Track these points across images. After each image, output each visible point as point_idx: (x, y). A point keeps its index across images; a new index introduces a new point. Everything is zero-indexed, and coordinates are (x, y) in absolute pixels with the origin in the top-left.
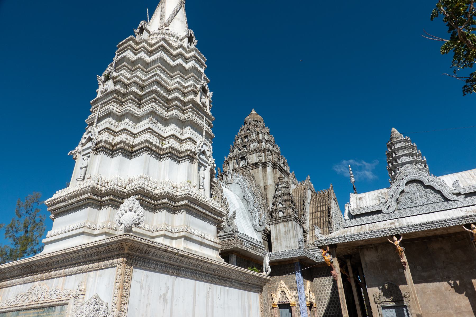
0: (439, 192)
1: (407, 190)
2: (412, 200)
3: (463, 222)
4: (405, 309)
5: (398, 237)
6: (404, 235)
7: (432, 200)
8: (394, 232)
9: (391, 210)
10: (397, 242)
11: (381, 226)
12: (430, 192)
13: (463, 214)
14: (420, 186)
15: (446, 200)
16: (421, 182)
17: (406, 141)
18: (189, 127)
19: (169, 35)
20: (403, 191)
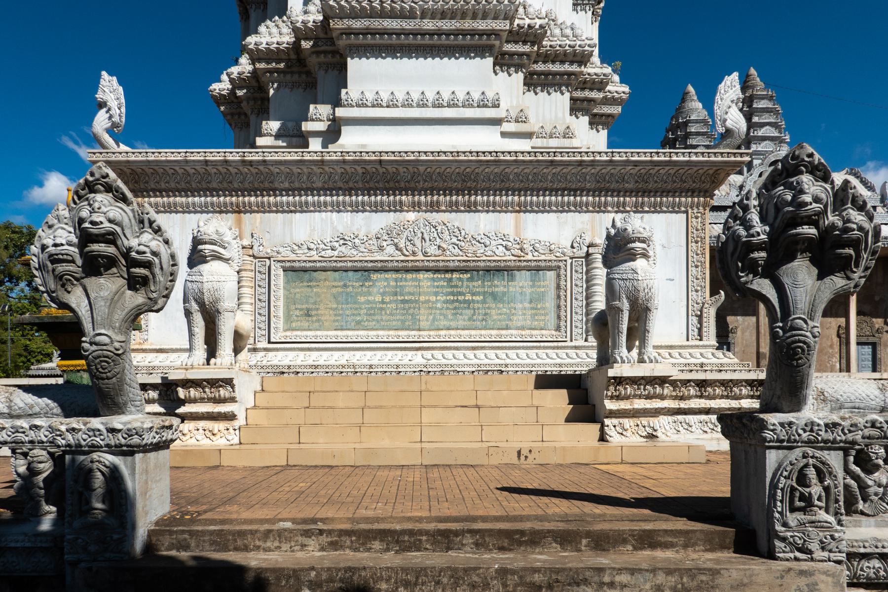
17: (770, 98)
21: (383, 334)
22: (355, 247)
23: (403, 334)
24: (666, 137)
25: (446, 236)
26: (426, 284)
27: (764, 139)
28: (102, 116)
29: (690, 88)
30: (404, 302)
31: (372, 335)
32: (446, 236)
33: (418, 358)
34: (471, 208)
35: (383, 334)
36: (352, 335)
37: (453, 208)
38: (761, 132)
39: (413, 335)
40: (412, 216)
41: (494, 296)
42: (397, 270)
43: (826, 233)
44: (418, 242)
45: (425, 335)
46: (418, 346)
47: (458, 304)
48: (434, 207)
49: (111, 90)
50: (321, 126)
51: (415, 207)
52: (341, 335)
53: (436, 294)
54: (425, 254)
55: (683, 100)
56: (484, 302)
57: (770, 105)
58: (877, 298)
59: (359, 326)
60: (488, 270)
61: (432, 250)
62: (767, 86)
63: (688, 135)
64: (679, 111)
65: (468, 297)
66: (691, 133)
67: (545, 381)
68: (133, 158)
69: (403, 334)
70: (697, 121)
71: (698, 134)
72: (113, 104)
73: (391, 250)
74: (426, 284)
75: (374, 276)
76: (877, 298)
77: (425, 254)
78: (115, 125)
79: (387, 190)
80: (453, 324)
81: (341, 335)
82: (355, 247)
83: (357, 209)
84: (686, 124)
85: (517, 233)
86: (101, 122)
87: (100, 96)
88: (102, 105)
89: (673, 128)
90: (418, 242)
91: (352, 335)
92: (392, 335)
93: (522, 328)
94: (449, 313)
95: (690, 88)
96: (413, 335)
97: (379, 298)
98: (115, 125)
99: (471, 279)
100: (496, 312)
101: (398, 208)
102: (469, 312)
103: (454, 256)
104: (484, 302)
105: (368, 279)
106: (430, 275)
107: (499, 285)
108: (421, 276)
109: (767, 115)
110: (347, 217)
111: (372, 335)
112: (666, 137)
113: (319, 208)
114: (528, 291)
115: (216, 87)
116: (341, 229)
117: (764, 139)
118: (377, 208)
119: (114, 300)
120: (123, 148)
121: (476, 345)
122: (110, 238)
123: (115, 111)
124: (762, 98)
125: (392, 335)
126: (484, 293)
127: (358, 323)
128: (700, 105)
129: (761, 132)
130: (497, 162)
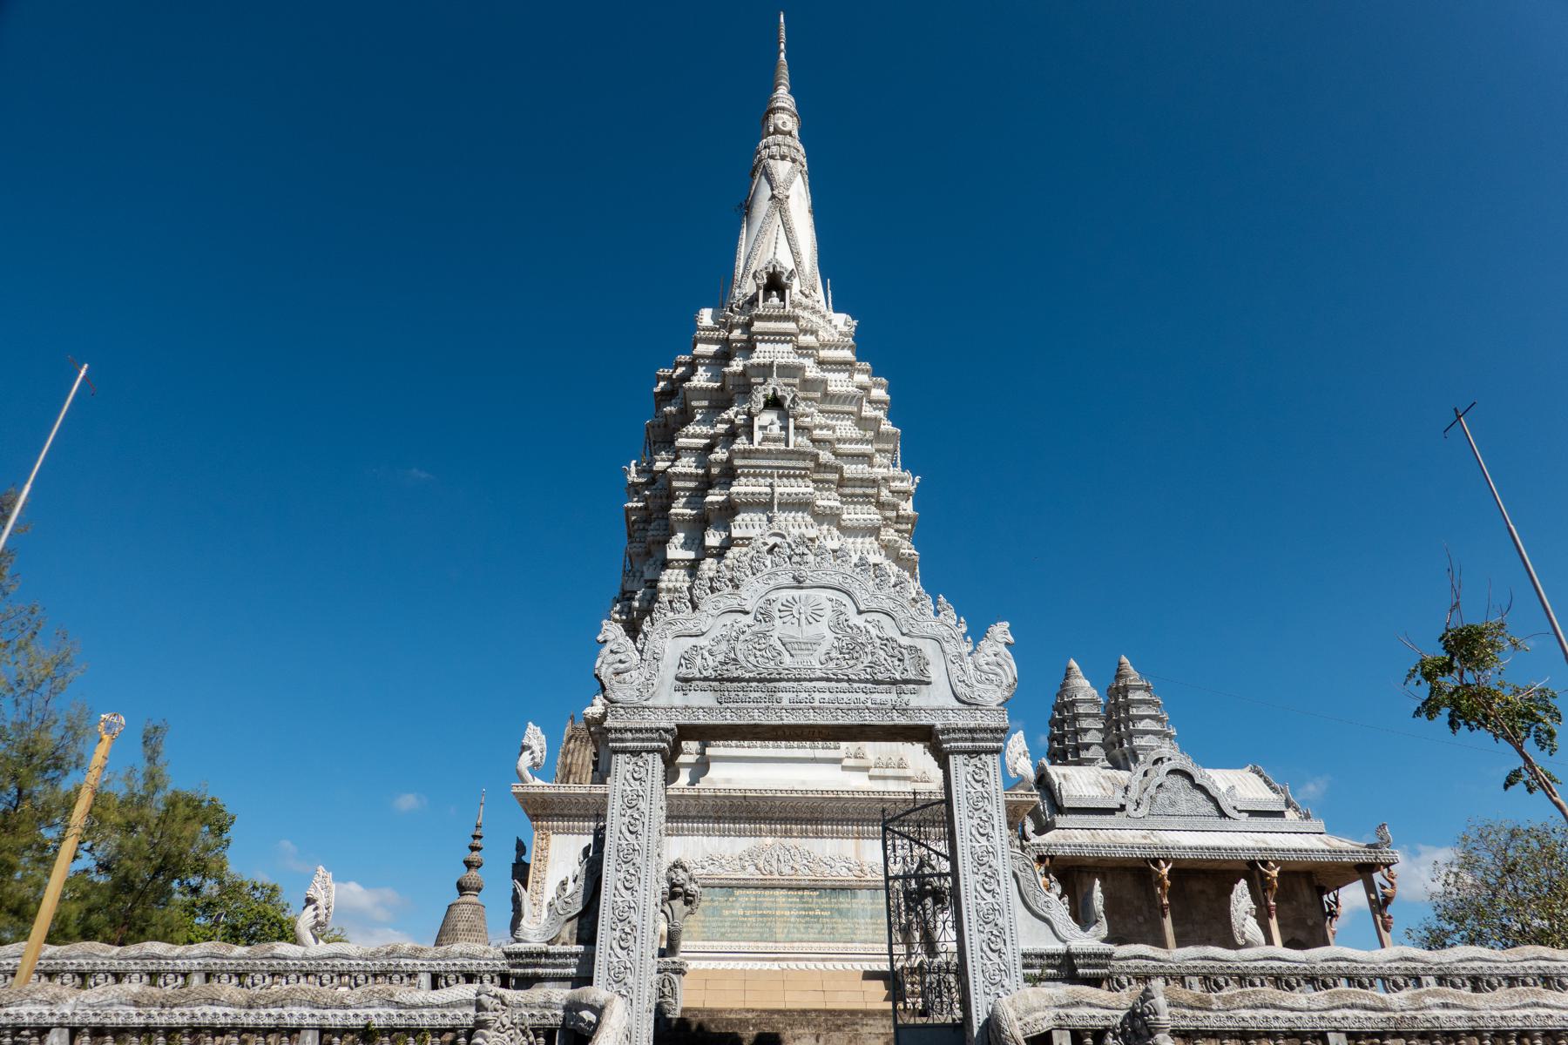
0: (1214, 800)
1: (1167, 784)
2: (1173, 804)
3: (1259, 857)
4: (947, 916)
5: (1167, 861)
6: (1176, 861)
7: (1202, 811)
8: (1162, 854)
9: (1140, 813)
10: (1165, 871)
11: (1103, 837)
12: (1200, 796)
13: (1250, 844)
14: (1186, 782)
15: (1223, 814)
16: (1189, 777)
17: (1147, 689)
18: (855, 323)
19: (273, 957)
20: (1160, 786)
21: (744, 946)
22: (721, 866)
23: (762, 946)
24: (1053, 717)
25: (798, 858)
26: (781, 900)
27: (1146, 732)
28: (526, 754)
29: (1073, 663)
30: (762, 916)
31: (735, 946)
32: (798, 858)
33: (775, 966)
34: (818, 835)
35: (744, 946)
36: (718, 945)
37: (804, 835)
38: (1141, 726)
39: (770, 946)
40: (769, 840)
41: (840, 911)
42: (756, 888)
43: (934, 889)
44: (774, 863)
45: (781, 946)
46: (776, 957)
47: (809, 919)
48: (787, 834)
49: (535, 736)
50: (691, 759)
51: (772, 833)
52: (708, 945)
53: (790, 909)
54: (780, 874)
55: (1067, 676)
56: (831, 917)
57: (1146, 696)
58: (1310, 923)
59: (723, 937)
60: (833, 889)
61: (786, 870)
62: (1142, 674)
63: (1076, 717)
64: (1064, 688)
65: (818, 912)
66: (1079, 715)
67: (870, 976)
68: (547, 791)
69: (762, 946)
70: (1085, 701)
71: (1088, 715)
72: (537, 748)
73: (751, 869)
74: (781, 900)
75: (737, 892)
76: (1310, 923)
77: (780, 874)
78: (536, 765)
79: (749, 820)
80: (805, 937)
81: (708, 945)
82: (721, 866)
83: (723, 834)
84: (1073, 703)
85: (858, 856)
86: (525, 760)
87: (526, 741)
88: (524, 748)
89: (1059, 708)
90: (774, 863)
91: (718, 945)
92: (752, 946)
93: (865, 942)
94: (801, 926)
95: (1073, 663)
96: (770, 946)
97: (741, 912)
98: (536, 765)
99: (820, 896)
100: (842, 925)
101: (758, 834)
102: (819, 926)
103: (804, 876)
104: (831, 917)
105: (732, 895)
106: (784, 892)
107: (844, 901)
108: (777, 892)
109: (1144, 707)
110: (715, 840)
111: (735, 946)
112: (1053, 717)
113: (692, 832)
114: (869, 907)
115: (589, 711)
116: (710, 851)
117: (1146, 732)
118: (740, 834)
119: (681, 910)
120: (538, 782)
121: (826, 957)
122: (681, 886)
123: (538, 754)
124: (1138, 688)
125: (752, 946)
126: (831, 909)
127: (723, 934)
128: (1087, 683)
129: (1141, 726)
130: (839, 799)
